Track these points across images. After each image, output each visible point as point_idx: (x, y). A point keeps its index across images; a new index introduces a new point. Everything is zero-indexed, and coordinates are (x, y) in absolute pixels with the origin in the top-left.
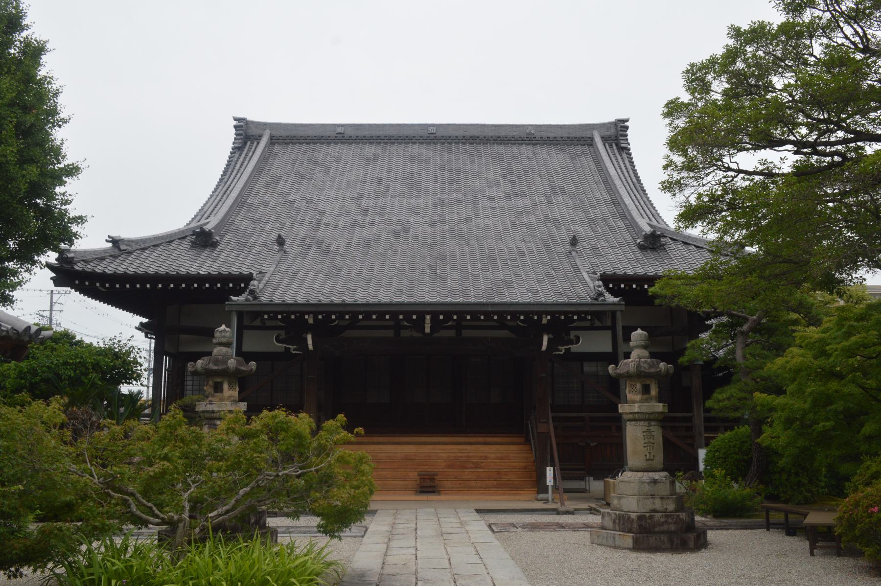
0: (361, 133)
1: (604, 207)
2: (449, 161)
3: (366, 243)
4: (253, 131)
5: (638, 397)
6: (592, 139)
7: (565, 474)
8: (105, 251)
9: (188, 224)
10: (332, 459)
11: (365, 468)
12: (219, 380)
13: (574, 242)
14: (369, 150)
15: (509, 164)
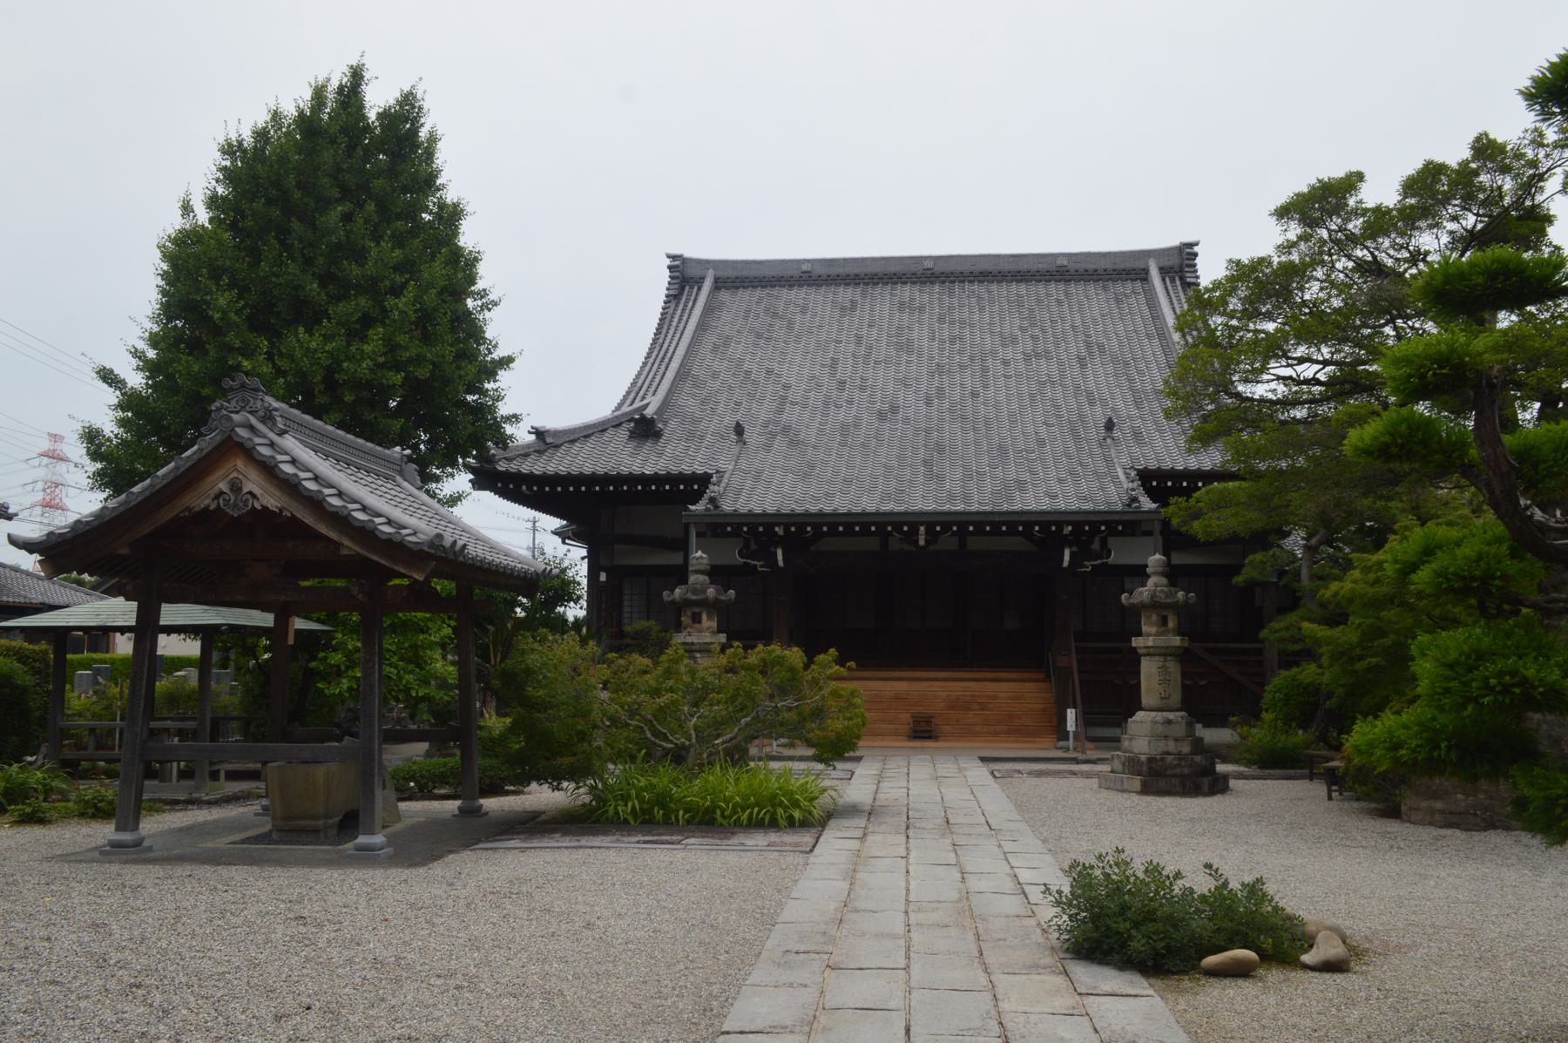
0: (833, 271)
1: (1156, 372)
2: (951, 308)
3: (844, 429)
4: (694, 272)
5: (1153, 630)
6: (1146, 271)
7: (1087, 720)
8: (528, 446)
9: (617, 409)
10: (825, 692)
11: (857, 701)
12: (697, 610)
13: (1110, 426)
14: (846, 294)
15: (1031, 311)
